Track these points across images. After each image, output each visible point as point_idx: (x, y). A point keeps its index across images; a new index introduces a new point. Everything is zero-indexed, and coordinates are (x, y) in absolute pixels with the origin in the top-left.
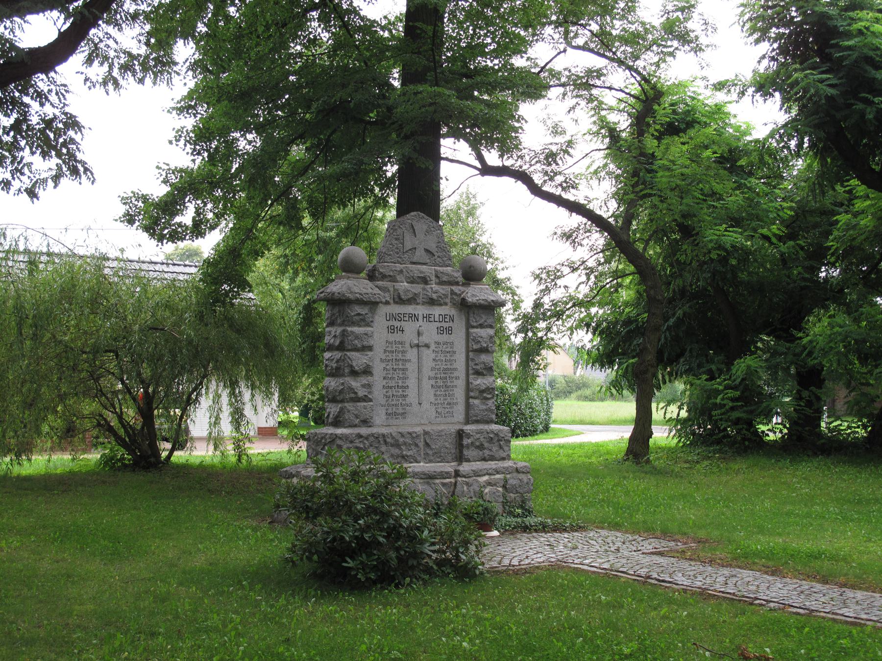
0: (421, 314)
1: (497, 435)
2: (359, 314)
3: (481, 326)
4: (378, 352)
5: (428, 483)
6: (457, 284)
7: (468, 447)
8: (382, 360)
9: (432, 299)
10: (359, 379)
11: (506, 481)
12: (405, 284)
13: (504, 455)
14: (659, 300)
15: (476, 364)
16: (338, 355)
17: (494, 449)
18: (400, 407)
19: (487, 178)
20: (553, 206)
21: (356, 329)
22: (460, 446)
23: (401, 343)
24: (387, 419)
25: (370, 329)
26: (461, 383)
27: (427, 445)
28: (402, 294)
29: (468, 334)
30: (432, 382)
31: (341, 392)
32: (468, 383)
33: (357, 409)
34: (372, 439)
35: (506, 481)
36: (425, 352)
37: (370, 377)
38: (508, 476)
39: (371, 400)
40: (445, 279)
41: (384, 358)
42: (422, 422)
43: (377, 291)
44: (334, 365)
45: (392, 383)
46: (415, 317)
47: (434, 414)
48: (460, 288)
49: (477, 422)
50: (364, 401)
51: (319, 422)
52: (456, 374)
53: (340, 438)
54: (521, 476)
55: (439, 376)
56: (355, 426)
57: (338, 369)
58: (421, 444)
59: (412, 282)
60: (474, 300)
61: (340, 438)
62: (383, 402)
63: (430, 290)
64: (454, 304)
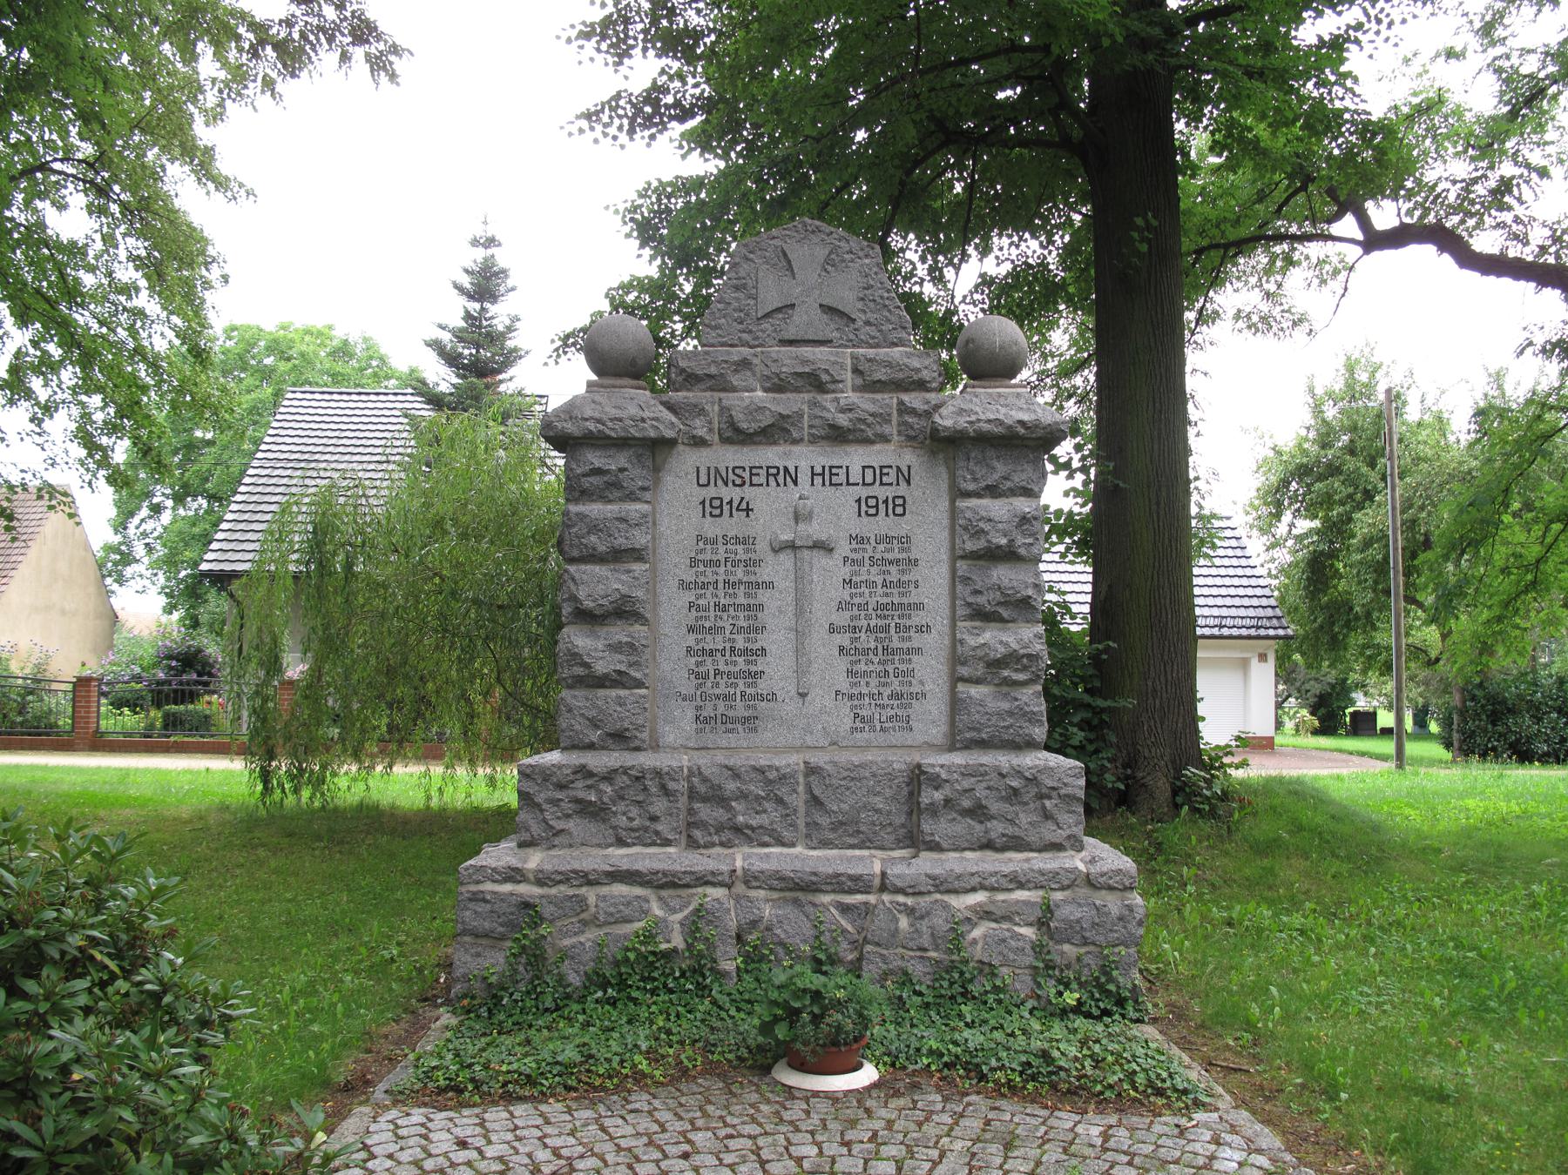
0: (804, 466)
1: (1033, 781)
3: (993, 491)
4: (674, 560)
5: (796, 902)
7: (933, 810)
8: (684, 585)
9: (833, 427)
10: (602, 631)
11: (1048, 909)
12: (760, 393)
15: (977, 592)
17: (1024, 819)
19: (1377, 255)
20: (1506, 282)
22: (914, 808)
27: (815, 801)
29: (954, 513)
32: (955, 642)
33: (595, 706)
35: (1048, 909)
36: (819, 560)
39: (639, 684)
40: (881, 374)
42: (809, 741)
52: (918, 618)
54: (1101, 898)
55: (864, 623)
56: (591, 746)
58: (798, 800)
60: (962, 422)
62: (688, 687)
63: (832, 407)
64: (910, 438)
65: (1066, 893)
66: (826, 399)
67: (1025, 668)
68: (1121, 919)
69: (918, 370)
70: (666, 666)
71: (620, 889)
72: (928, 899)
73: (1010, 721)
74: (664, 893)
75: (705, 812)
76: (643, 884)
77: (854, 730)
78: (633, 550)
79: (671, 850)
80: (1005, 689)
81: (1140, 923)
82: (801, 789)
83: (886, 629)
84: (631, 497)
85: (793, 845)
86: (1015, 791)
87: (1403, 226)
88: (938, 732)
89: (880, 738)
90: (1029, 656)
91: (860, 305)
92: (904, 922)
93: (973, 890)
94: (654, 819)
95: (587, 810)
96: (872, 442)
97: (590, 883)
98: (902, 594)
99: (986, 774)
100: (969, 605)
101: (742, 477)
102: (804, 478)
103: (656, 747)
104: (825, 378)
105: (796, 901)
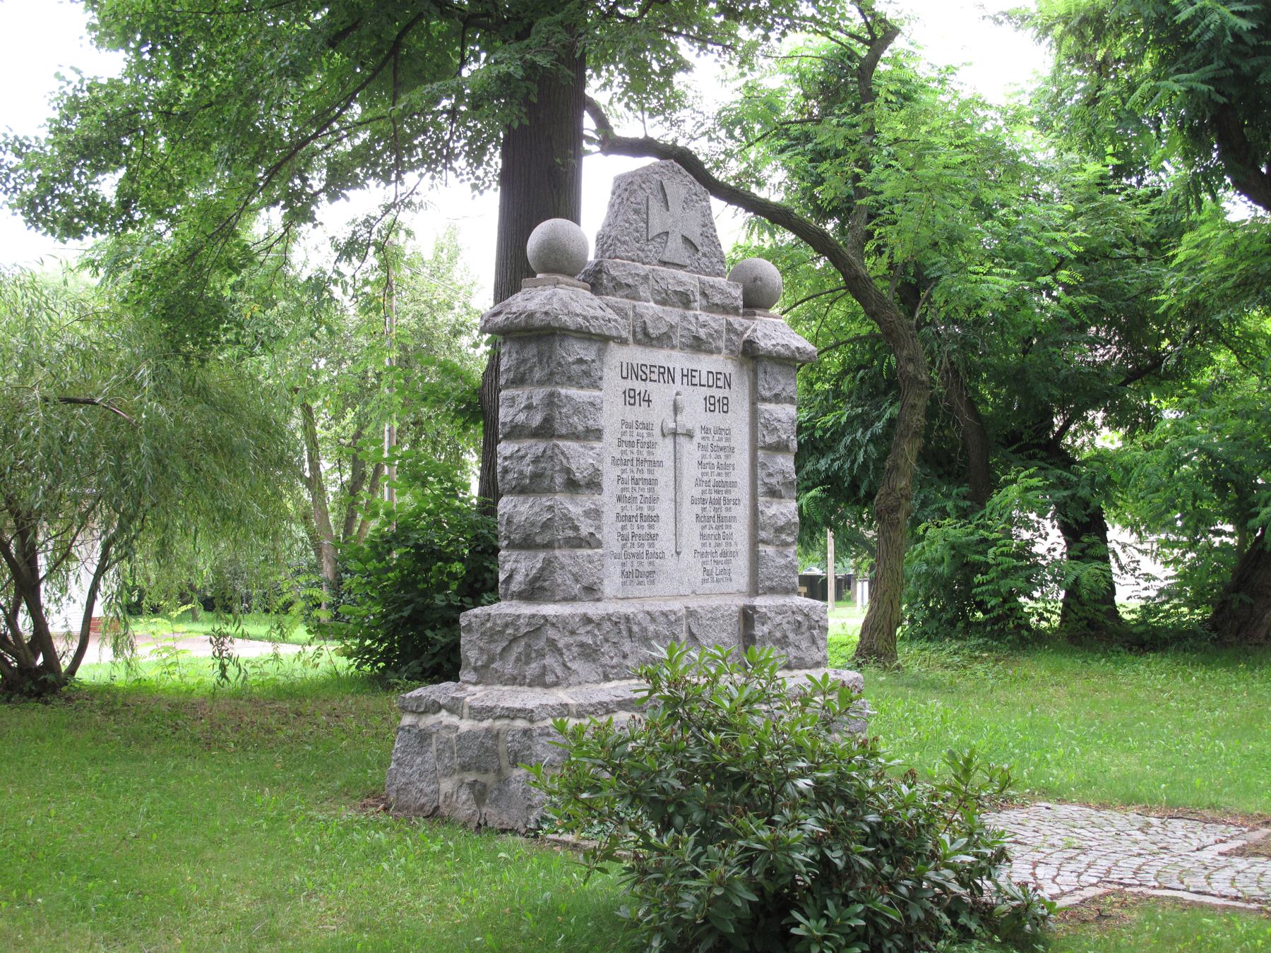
2: (580, 361)
3: (777, 399)
6: (735, 311)
8: (615, 462)
9: (697, 338)
12: (652, 304)
13: (818, 656)
14: (922, 383)
15: (770, 475)
16: (539, 446)
17: (804, 645)
18: (645, 561)
21: (573, 392)
22: (748, 639)
23: (647, 426)
24: (624, 584)
25: (596, 393)
26: (742, 512)
28: (649, 324)
29: (754, 414)
31: (546, 526)
32: (755, 512)
33: (577, 564)
34: (607, 626)
37: (596, 496)
40: (717, 299)
41: (618, 456)
43: (610, 314)
44: (529, 470)
45: (632, 510)
46: (667, 374)
47: (700, 573)
48: (740, 319)
49: (772, 590)
50: (590, 546)
51: (134, 610)
53: (553, 625)
55: (707, 496)
56: (574, 599)
57: (536, 476)
59: (663, 303)
61: (553, 625)
62: (617, 549)
63: (693, 320)
64: (732, 352)
77: (704, 581)
80: (781, 549)
87: (701, 164)
100: (765, 484)
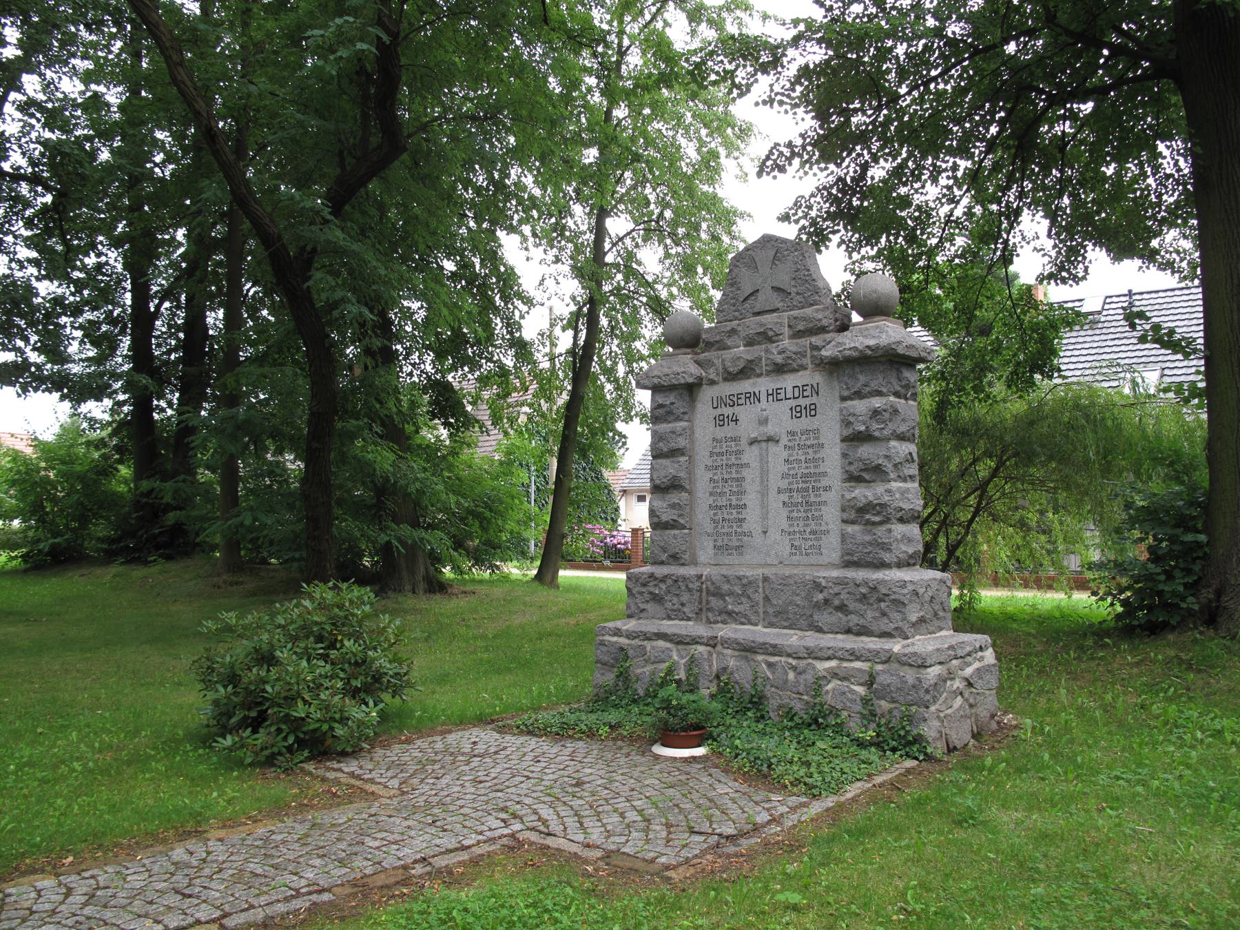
0: (763, 390)
4: (703, 456)
10: (668, 497)
17: (870, 614)
18: (734, 538)
23: (734, 439)
24: (716, 554)
27: (767, 599)
30: (784, 497)
36: (772, 448)
38: (879, 667)
45: (722, 501)
47: (788, 548)
52: (824, 482)
55: (795, 486)
56: (662, 563)
58: (759, 598)
62: (709, 528)
64: (818, 365)
65: (886, 666)
66: (773, 348)
67: (878, 513)
68: (914, 686)
69: (820, 320)
70: (700, 517)
71: (661, 644)
72: (805, 662)
73: (870, 548)
74: (680, 647)
75: (715, 603)
76: (671, 641)
78: (678, 449)
79: (691, 623)
80: (869, 527)
81: (927, 691)
82: (761, 590)
83: (807, 490)
84: (678, 419)
85: (756, 625)
86: (864, 596)
88: (835, 556)
89: (804, 560)
90: (880, 505)
91: (793, 283)
92: (791, 675)
93: (829, 658)
94: (683, 605)
95: (658, 599)
96: (798, 371)
97: (649, 639)
98: (815, 467)
99: (847, 584)
101: (733, 401)
102: (764, 398)
103: (694, 562)
104: (771, 333)
105: (746, 658)
